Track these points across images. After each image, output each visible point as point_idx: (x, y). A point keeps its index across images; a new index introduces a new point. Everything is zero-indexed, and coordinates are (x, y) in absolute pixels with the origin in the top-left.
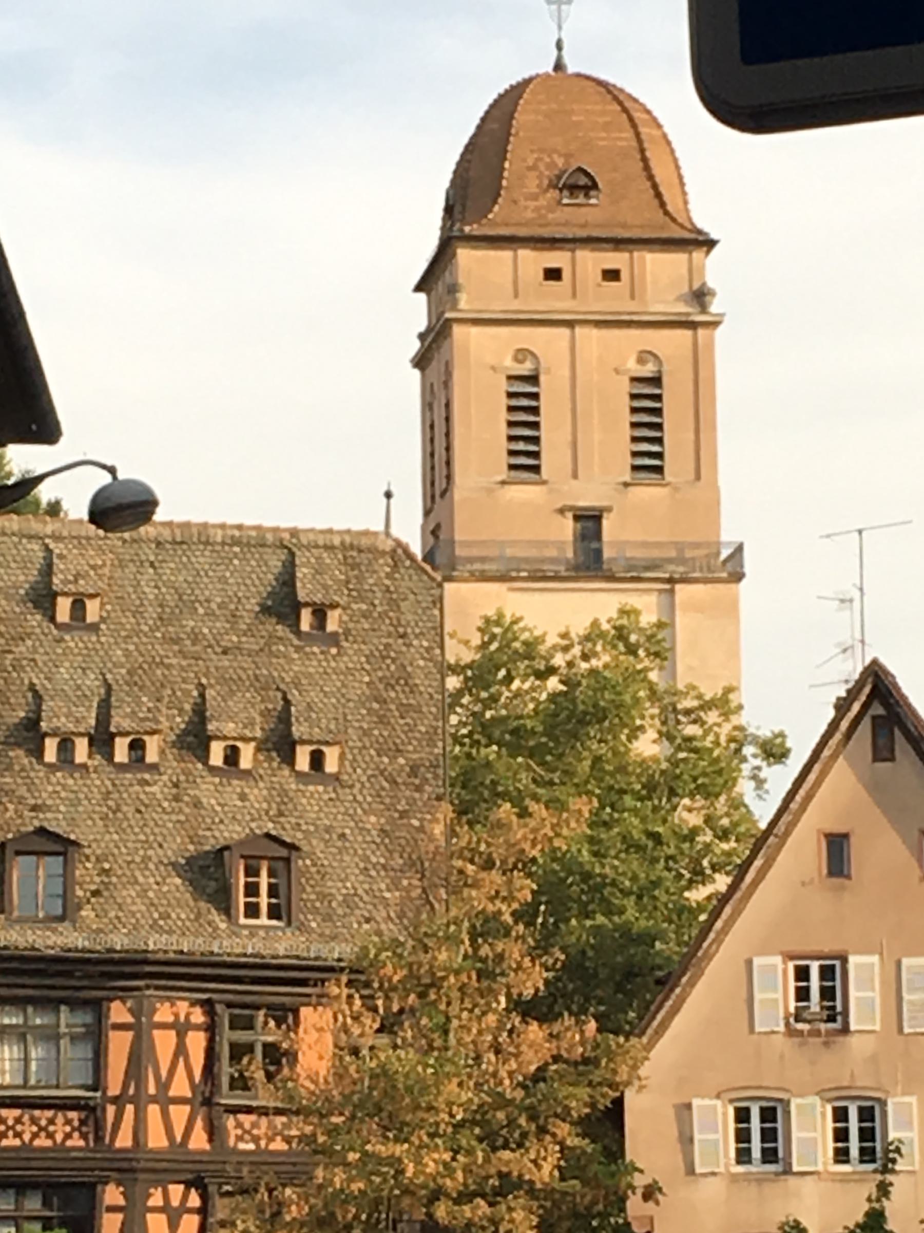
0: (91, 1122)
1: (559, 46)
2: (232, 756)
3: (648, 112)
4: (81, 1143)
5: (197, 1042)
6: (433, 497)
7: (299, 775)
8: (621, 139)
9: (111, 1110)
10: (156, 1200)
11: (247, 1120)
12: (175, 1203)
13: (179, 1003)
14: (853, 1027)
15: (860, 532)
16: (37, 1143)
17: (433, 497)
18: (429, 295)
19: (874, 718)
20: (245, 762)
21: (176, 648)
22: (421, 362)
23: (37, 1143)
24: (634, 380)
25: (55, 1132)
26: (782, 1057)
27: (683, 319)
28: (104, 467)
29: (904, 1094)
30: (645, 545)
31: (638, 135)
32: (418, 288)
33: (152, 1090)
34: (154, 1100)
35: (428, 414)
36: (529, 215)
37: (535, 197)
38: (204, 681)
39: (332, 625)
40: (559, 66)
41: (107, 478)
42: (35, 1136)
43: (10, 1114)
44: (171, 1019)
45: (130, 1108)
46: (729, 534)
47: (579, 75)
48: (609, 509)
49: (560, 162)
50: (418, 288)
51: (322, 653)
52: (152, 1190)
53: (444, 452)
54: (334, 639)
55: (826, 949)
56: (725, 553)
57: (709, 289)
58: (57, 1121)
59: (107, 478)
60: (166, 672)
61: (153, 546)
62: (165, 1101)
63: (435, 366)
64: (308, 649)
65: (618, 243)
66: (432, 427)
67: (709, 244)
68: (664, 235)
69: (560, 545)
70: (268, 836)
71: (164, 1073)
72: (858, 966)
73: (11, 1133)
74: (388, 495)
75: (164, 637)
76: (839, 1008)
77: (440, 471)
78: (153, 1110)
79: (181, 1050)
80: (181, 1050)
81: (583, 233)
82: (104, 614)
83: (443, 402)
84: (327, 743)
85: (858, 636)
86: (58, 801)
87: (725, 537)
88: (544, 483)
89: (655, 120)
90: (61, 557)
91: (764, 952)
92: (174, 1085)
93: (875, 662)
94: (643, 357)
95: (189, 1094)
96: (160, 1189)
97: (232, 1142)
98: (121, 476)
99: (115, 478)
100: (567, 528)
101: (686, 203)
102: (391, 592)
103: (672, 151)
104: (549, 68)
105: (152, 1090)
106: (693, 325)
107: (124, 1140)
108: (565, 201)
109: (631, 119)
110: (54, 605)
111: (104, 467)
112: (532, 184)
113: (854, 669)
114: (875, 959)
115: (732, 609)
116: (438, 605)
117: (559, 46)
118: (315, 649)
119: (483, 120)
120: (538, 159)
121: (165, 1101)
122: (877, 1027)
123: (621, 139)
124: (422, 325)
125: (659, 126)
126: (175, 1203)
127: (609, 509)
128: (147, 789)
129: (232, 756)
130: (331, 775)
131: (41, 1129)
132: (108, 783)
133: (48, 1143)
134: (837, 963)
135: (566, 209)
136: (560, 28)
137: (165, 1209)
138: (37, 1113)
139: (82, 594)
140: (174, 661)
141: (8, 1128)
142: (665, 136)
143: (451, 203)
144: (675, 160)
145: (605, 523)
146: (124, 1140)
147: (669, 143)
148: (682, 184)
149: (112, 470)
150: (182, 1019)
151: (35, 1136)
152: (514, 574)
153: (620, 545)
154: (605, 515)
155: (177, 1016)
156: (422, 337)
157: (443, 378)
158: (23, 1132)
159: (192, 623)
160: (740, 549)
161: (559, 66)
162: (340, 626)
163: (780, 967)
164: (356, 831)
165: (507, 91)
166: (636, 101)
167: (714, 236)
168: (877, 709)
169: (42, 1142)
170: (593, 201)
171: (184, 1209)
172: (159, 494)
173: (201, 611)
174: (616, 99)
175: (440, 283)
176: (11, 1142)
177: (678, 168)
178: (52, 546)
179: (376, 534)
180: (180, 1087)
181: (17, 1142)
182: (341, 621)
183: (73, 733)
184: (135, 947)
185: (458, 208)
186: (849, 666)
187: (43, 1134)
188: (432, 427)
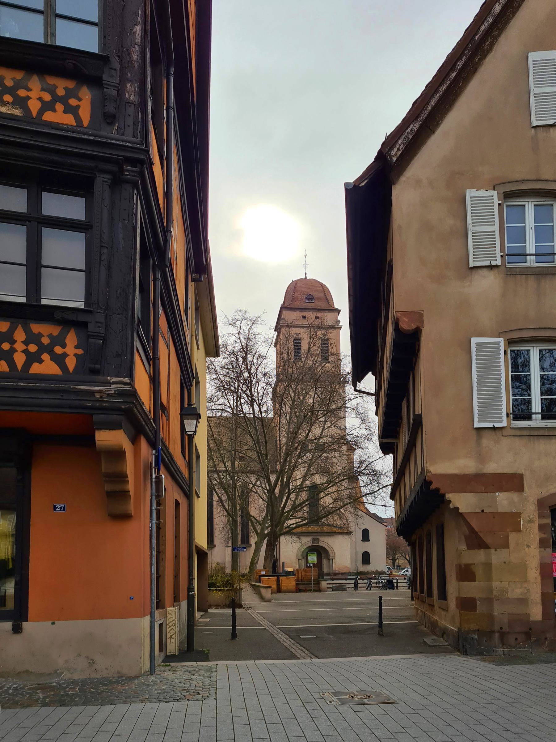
1: (306, 274)
8: (319, 289)
36: (299, 304)
37: (300, 301)
40: (306, 278)
104: (304, 278)
117: (306, 274)
136: (306, 270)
161: (306, 278)
167: (340, 309)
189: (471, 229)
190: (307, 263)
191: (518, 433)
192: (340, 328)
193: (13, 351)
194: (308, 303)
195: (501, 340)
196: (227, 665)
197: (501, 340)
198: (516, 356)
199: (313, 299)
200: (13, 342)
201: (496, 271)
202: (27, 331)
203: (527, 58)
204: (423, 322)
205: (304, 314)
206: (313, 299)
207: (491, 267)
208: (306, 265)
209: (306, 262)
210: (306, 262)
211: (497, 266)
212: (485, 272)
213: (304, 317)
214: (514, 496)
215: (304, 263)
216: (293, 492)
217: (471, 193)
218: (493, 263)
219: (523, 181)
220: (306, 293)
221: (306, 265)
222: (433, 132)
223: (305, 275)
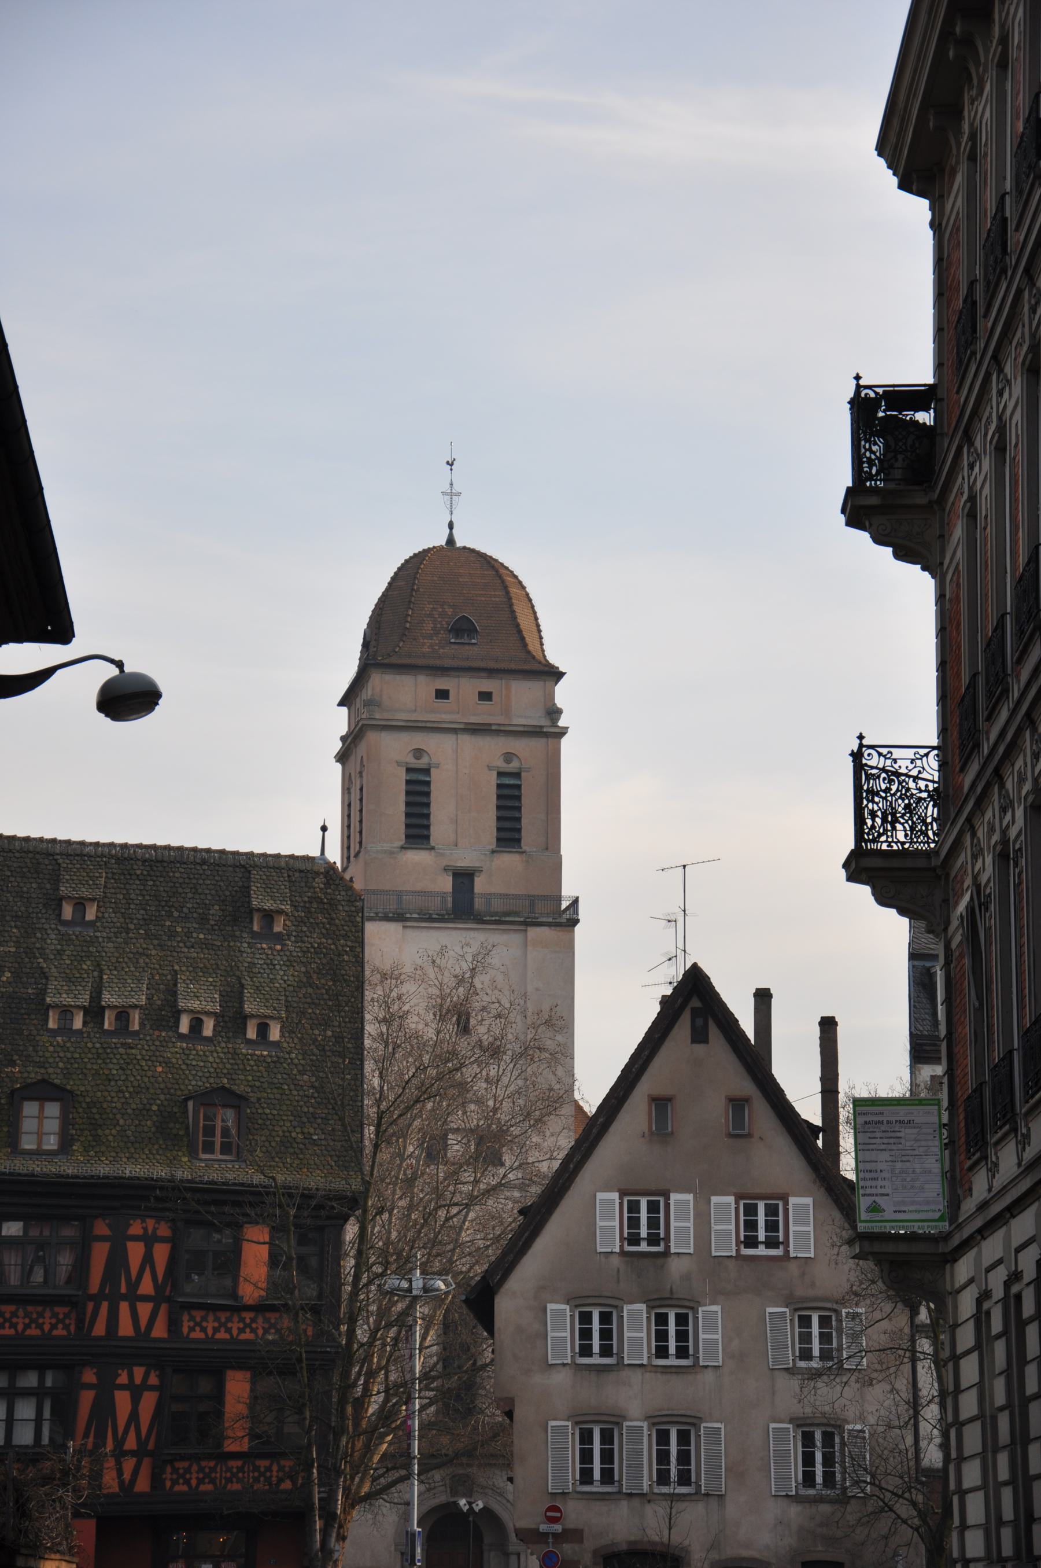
0: (73, 1315)
1: (451, 526)
2: (196, 1025)
3: (516, 577)
4: (65, 1333)
5: (161, 1253)
6: (348, 858)
7: (249, 1042)
8: (495, 596)
9: (90, 1306)
10: (123, 1379)
11: (198, 1315)
12: (138, 1380)
13: (148, 1220)
14: (673, 1250)
15: (684, 866)
16: (28, 1332)
17: (348, 858)
18: (349, 709)
19: (693, 1010)
20: (208, 1030)
21: (156, 942)
22: (342, 757)
23: (28, 1332)
24: (500, 774)
25: (44, 1323)
26: (618, 1270)
27: (538, 730)
28: (112, 661)
29: (712, 1303)
30: (506, 896)
31: (508, 593)
32: (341, 704)
33: (123, 1290)
34: (124, 1297)
35: (346, 796)
36: (426, 649)
37: (430, 637)
38: (177, 968)
39: (278, 928)
40: (451, 541)
41: (114, 671)
42: (27, 1326)
43: (8, 1309)
44: (141, 1232)
45: (105, 1306)
46: (568, 890)
47: (465, 548)
48: (479, 870)
49: (449, 611)
50: (341, 704)
51: (270, 948)
52: (120, 1372)
53: (358, 824)
54: (279, 937)
55: (653, 1187)
56: (564, 904)
57: (558, 708)
58: (49, 1326)
59: (114, 671)
60: (147, 960)
61: (140, 863)
62: (134, 1298)
63: (353, 763)
64: (259, 946)
65: (492, 673)
66: (349, 805)
67: (558, 675)
68: (526, 667)
69: (443, 895)
70: (223, 1088)
71: (134, 1273)
72: (676, 1202)
73: (7, 1325)
74: (324, 829)
75: (146, 934)
76: (662, 1236)
77: (355, 837)
78: (124, 1307)
79: (148, 1259)
80: (148, 1259)
81: (466, 664)
82: (100, 915)
83: (358, 787)
84: (271, 1018)
85: (681, 945)
86: (57, 1060)
87: (565, 892)
88: (433, 848)
89: (520, 582)
90: (66, 869)
91: (607, 1189)
92: (142, 1285)
93: (695, 967)
94: (508, 757)
95: (153, 1293)
96: (126, 1371)
97: (185, 1330)
98: (127, 669)
99: (122, 671)
100: (446, 884)
101: (542, 644)
102: (324, 903)
103: (533, 607)
104: (443, 543)
105: (123, 1290)
106: (547, 735)
107: (100, 1329)
108: (453, 640)
109: (503, 581)
110: (60, 906)
111: (112, 661)
112: (428, 627)
113: (676, 972)
114: (690, 1197)
115: (569, 948)
116: (360, 915)
117: (451, 526)
118: (264, 946)
119: (393, 578)
120: (434, 609)
121: (134, 1298)
122: (691, 1251)
123: (495, 596)
124: (344, 730)
125: (524, 588)
126: (138, 1380)
127: (479, 870)
128: (129, 1051)
129: (196, 1025)
130: (274, 1042)
131: (32, 1321)
132: (98, 1045)
133: (38, 1332)
134: (662, 1200)
135: (453, 646)
136: (452, 514)
137: (131, 1387)
138: (30, 1308)
139: (83, 898)
140: (153, 952)
141: (5, 1320)
142: (527, 595)
143: (368, 639)
144: (535, 613)
145: (477, 880)
146: (100, 1329)
147: (530, 600)
148: (539, 631)
149: (120, 665)
150: (150, 1232)
151: (27, 1326)
152: (408, 916)
153: (488, 897)
154: (477, 874)
155: (145, 1229)
156: (343, 739)
157: (358, 770)
158: (17, 1323)
159: (168, 923)
160: (576, 901)
161: (451, 541)
162: (284, 929)
163: (617, 1201)
164: (292, 1087)
165: (411, 558)
166: (507, 568)
167: (562, 669)
168: (695, 1003)
169: (33, 1331)
170: (473, 641)
171: (145, 1386)
172: (162, 688)
173: (176, 914)
174: (493, 567)
175: (358, 700)
176: (8, 1331)
177: (536, 619)
178: (60, 861)
179: (313, 858)
180: (146, 1287)
181: (12, 1332)
182: (285, 925)
183: (71, 1006)
184: (115, 1174)
185: (373, 643)
186: (672, 971)
187: (33, 1326)
188: (349, 805)
189: (550, 1334)
190: (457, 488)
191: (580, 1496)
192: (563, 732)
193: (271, 1476)
194: (456, 647)
195: (569, 1424)
196: (828, 1025)
197: (569, 1424)
198: (582, 1432)
199: (472, 631)
200: (271, 1471)
201: (567, 1367)
202: (278, 1464)
203: (595, 1196)
204: (514, 1405)
205: (442, 684)
206: (472, 631)
207: (564, 1365)
208: (451, 494)
209: (451, 484)
210: (451, 484)
211: (567, 1364)
212: (561, 1368)
213: (442, 694)
214: (576, 1547)
215: (446, 488)
216: (373, 1302)
217: (550, 1306)
218: (565, 1362)
219: (588, 1297)
220: (450, 611)
221: (451, 494)
222: (525, 1254)
223: (448, 531)
